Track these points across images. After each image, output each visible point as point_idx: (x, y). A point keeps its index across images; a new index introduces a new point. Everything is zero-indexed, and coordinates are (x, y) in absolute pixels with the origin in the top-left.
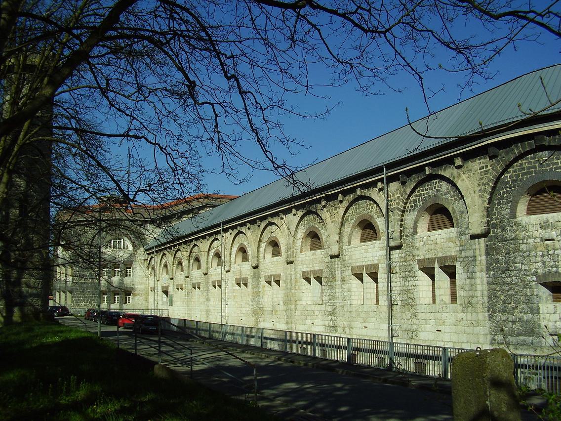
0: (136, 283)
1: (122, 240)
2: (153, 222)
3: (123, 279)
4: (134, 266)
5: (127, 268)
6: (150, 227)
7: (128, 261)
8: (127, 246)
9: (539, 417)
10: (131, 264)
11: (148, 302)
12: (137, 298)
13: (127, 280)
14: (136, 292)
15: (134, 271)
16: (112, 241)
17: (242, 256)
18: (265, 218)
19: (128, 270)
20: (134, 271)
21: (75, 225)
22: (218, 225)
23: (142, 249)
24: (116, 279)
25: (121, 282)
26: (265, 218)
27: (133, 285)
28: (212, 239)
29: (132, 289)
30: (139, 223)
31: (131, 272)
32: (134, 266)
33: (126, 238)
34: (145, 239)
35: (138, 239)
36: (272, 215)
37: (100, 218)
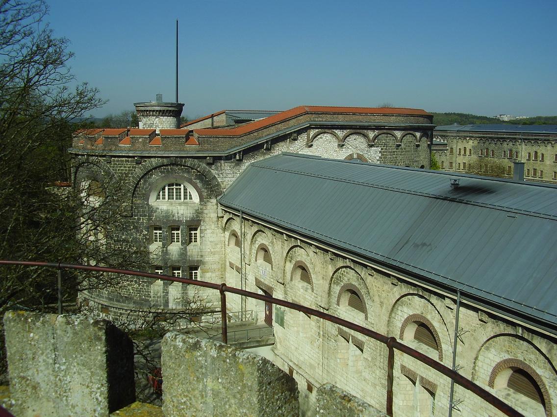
1: (182, 186)
2: (228, 158)
4: (203, 228)
5: (191, 229)
6: (226, 166)
7: (192, 220)
16: (167, 188)
19: (193, 232)
24: (175, 248)
25: (183, 253)
34: (218, 185)
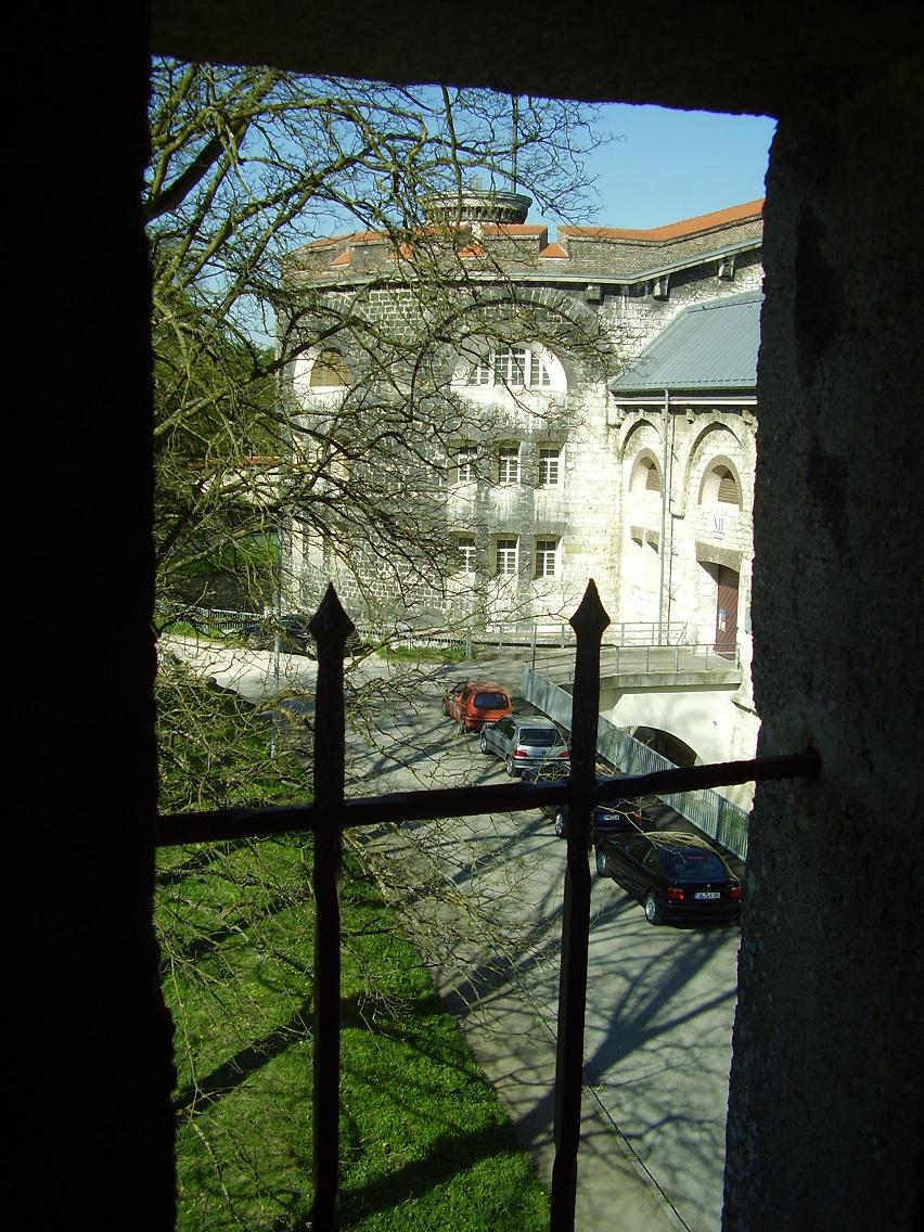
0: (579, 508)
3: (531, 495)
5: (544, 454)
8: (546, 376)
9: (295, 648)
10: (563, 440)
11: (618, 575)
12: (578, 558)
13: (548, 500)
14: (578, 539)
15: (570, 465)
17: (646, 479)
18: (707, 409)
19: (549, 460)
20: (570, 465)
21: (343, 114)
22: (660, 393)
23: (601, 387)
24: (505, 497)
25: (525, 507)
26: (707, 409)
27: (567, 514)
28: (702, 422)
29: (564, 528)
30: (592, 296)
31: (561, 467)
32: (573, 448)
33: (538, 346)
35: (587, 349)
36: (725, 409)
37: (455, 198)
